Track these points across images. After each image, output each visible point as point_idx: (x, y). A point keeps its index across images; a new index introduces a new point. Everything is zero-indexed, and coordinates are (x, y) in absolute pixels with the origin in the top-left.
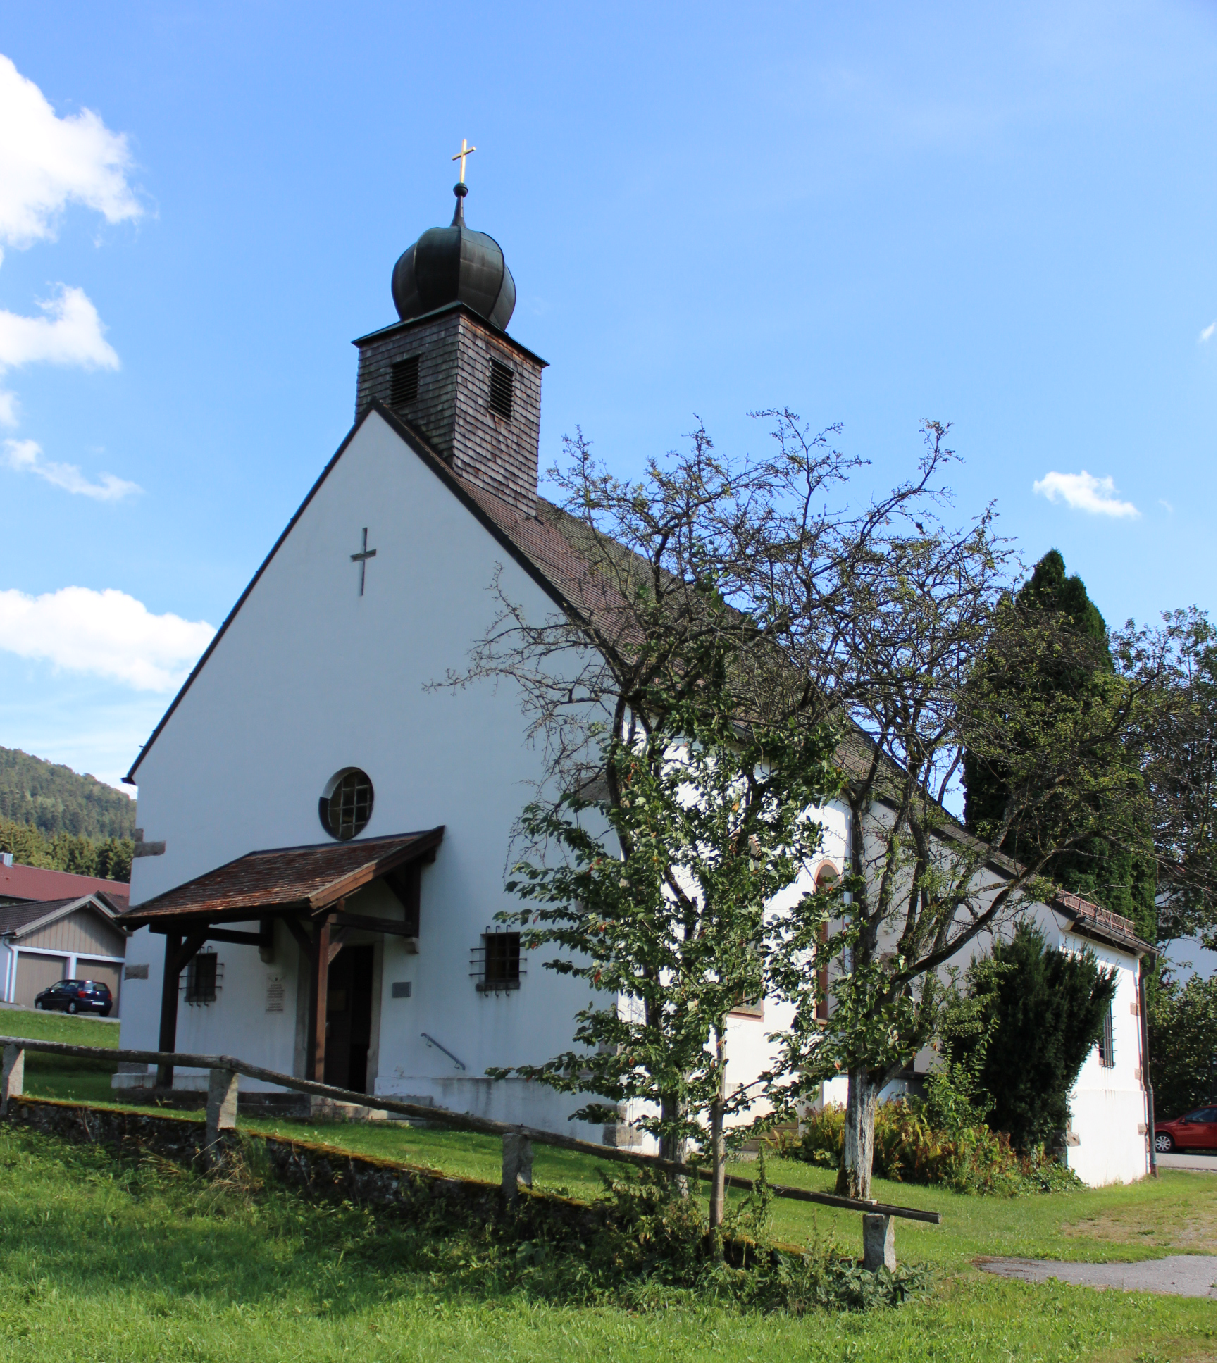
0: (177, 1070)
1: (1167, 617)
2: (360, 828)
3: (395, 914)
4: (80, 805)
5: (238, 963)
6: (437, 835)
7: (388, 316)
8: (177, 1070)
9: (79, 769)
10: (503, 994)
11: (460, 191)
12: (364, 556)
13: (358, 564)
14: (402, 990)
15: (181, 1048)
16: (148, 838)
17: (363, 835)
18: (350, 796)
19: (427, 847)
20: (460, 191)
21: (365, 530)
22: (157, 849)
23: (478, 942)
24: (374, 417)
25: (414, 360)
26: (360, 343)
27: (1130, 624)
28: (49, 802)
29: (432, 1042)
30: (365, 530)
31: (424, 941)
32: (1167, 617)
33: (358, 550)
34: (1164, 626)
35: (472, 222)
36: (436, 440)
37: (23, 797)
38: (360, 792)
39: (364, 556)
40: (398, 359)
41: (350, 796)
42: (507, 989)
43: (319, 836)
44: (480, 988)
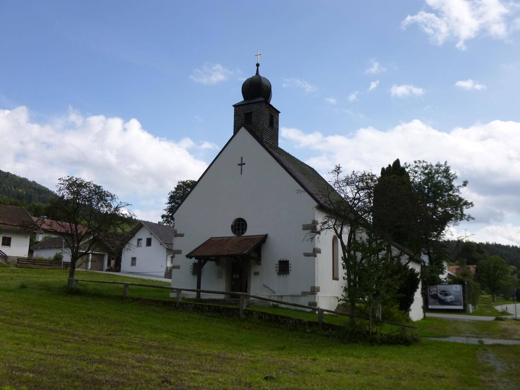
0: (201, 293)
1: (415, 162)
2: (243, 233)
3: (254, 255)
4: (31, 191)
5: (209, 267)
6: (266, 236)
7: (240, 99)
8: (201, 293)
9: (31, 179)
10: (285, 275)
11: (258, 65)
12: (242, 164)
13: (240, 166)
14: (257, 274)
15: (202, 288)
16: (178, 232)
17: (244, 235)
18: (240, 225)
19: (264, 239)
20: (258, 65)
21: (242, 158)
22: (182, 235)
23: (277, 263)
24: (243, 130)
25: (251, 113)
26: (234, 106)
27: (405, 163)
28: (20, 191)
29: (265, 286)
30: (242, 158)
31: (263, 261)
32: (415, 162)
33: (240, 163)
34: (414, 165)
35: (261, 74)
36: (258, 135)
37: (12, 189)
38: (242, 224)
39: (242, 164)
40: (246, 112)
41: (240, 225)
42: (286, 274)
43: (230, 234)
44: (278, 274)
